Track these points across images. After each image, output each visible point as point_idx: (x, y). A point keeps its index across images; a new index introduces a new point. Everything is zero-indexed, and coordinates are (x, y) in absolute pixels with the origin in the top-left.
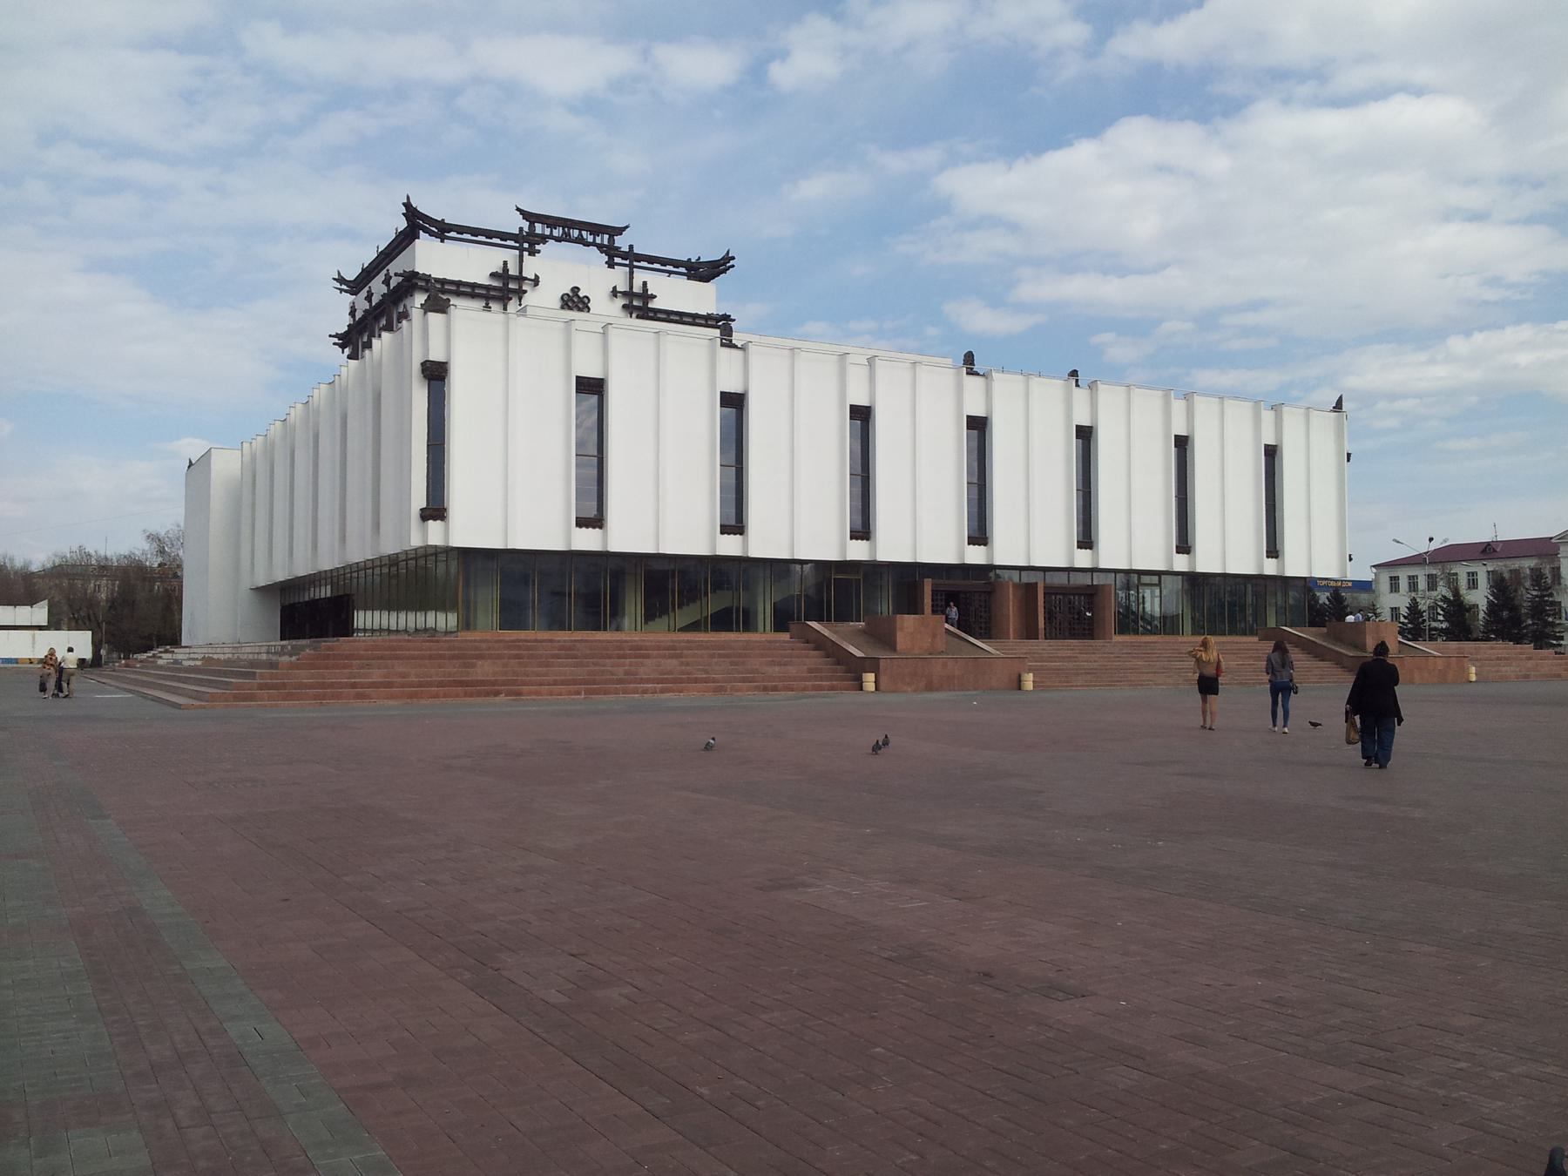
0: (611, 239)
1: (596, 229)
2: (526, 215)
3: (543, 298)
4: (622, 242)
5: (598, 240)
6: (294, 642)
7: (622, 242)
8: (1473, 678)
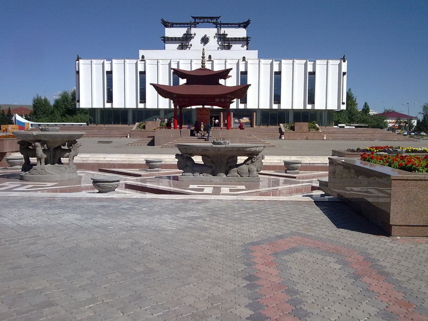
0: (217, 20)
1: (212, 18)
2: (193, 17)
3: (196, 42)
4: (219, 21)
5: (213, 21)
6: (107, 126)
7: (219, 21)
8: (325, 138)
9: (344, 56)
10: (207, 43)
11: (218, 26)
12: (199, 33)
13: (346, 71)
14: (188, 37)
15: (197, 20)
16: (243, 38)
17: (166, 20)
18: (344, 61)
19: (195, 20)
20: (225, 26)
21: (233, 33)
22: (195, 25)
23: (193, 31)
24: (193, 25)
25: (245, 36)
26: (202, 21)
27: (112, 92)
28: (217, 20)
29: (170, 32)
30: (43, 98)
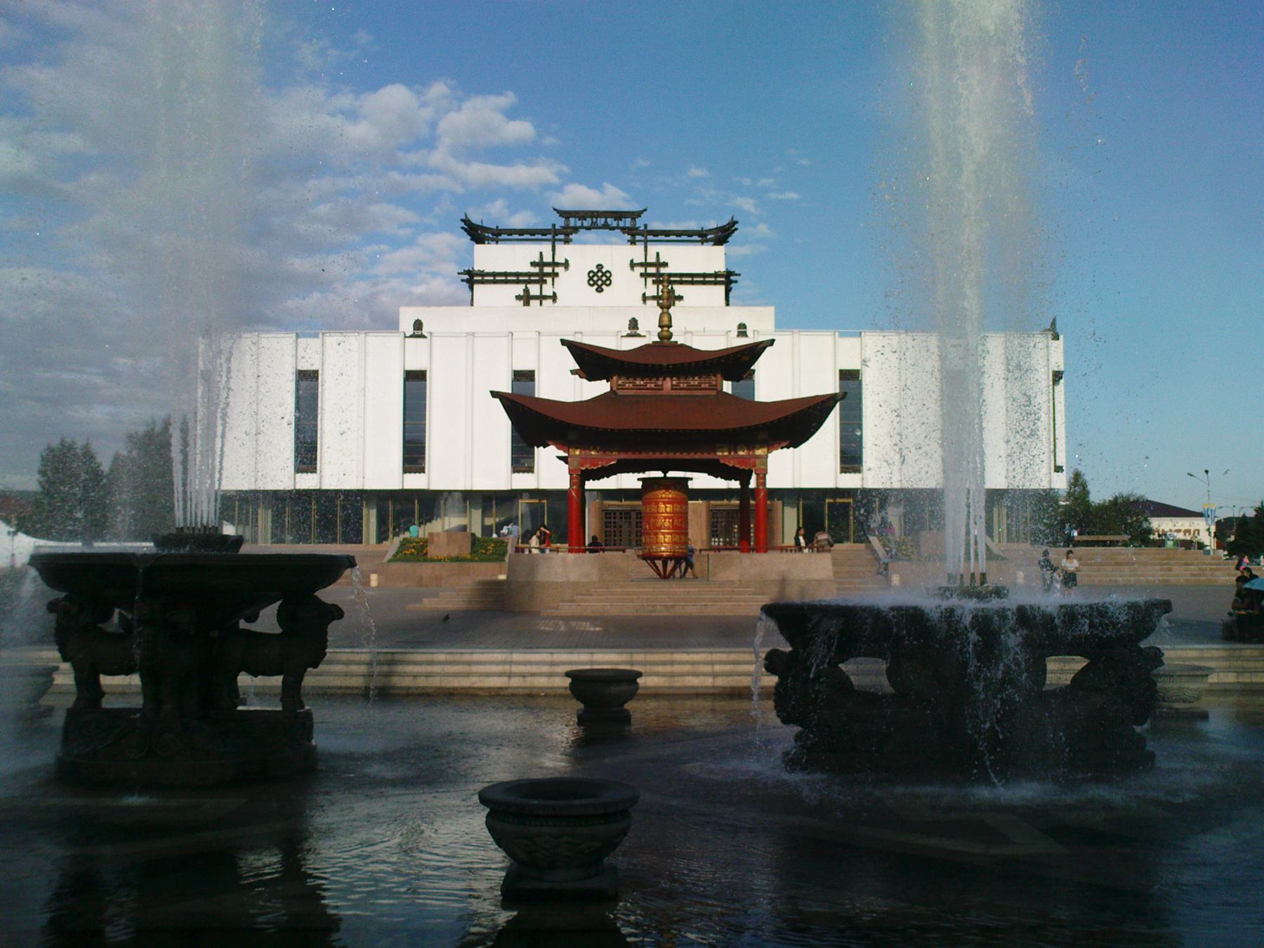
1: (619, 215)
4: (640, 223)
5: (621, 224)
7: (640, 223)
9: (1053, 324)
11: (638, 238)
12: (581, 255)
13: (1062, 369)
14: (543, 272)
16: (716, 275)
17: (476, 219)
18: (1056, 337)
20: (526, 236)
21: (681, 258)
22: (563, 234)
23: (563, 252)
24: (562, 237)
25: (721, 267)
26: (587, 223)
27: (861, 437)
29: (489, 257)
30: (80, 443)
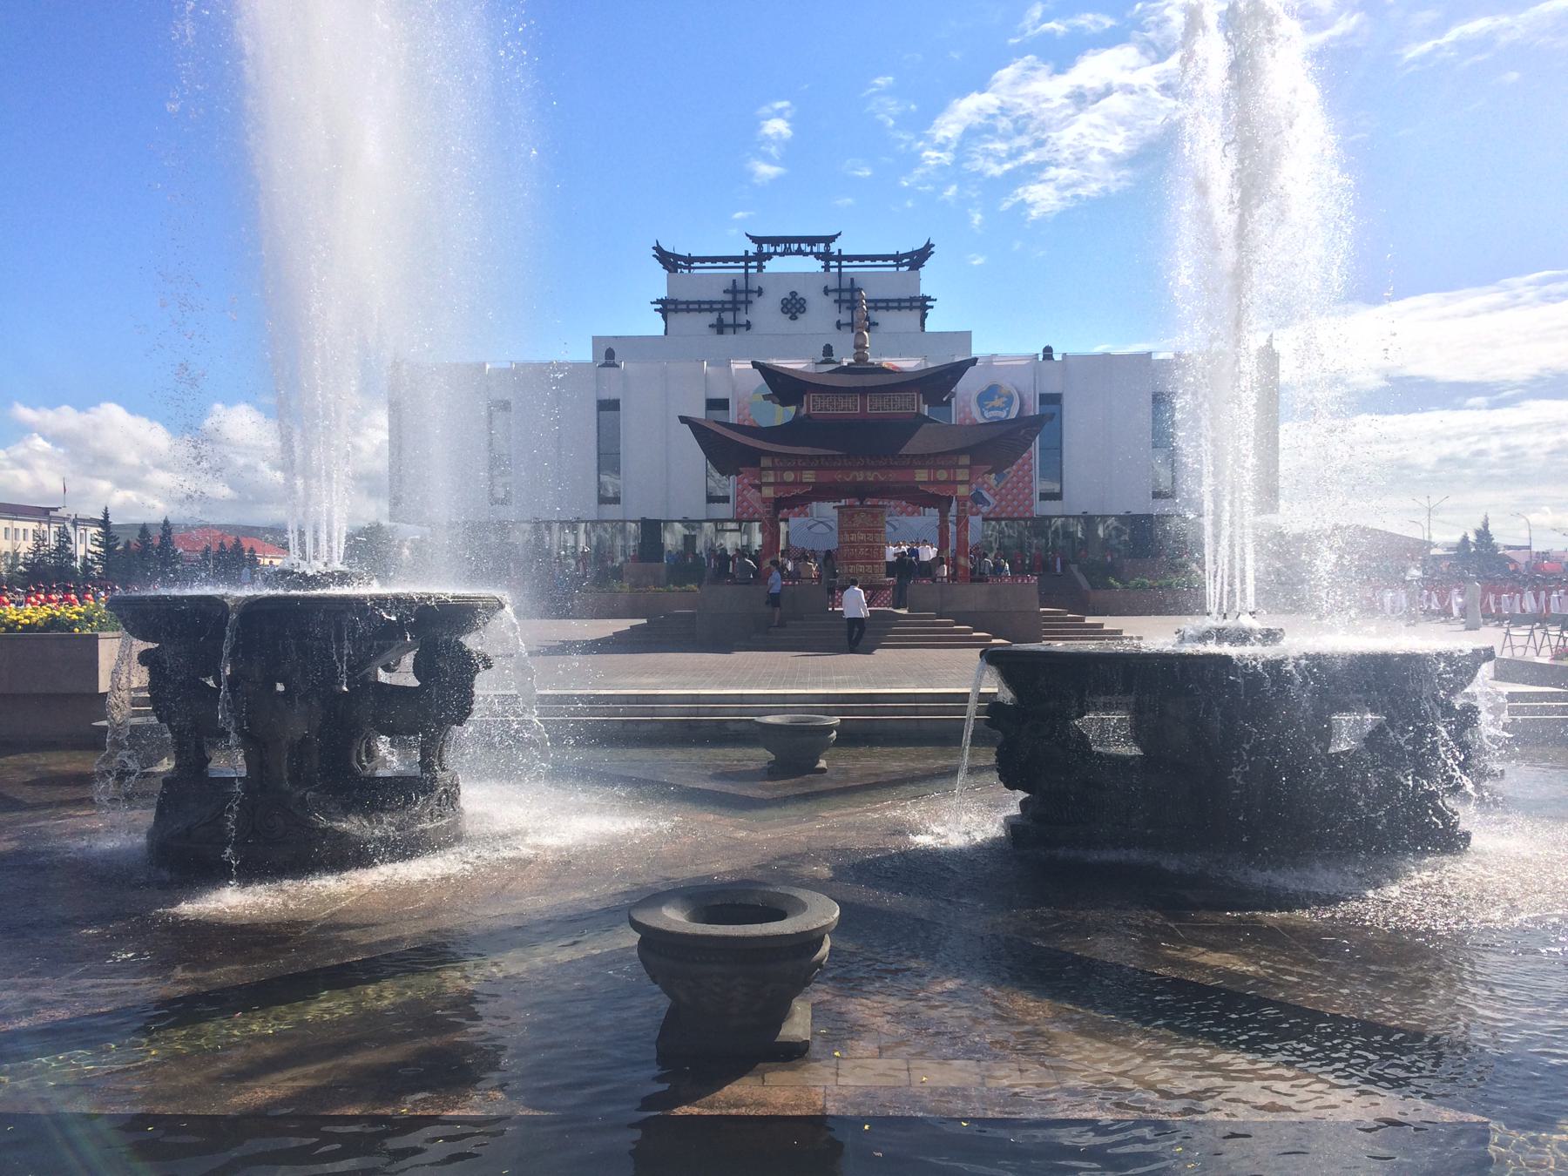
1: (812, 241)
2: (755, 239)
4: (834, 248)
5: (815, 249)
10: (1378, 301)
11: (832, 263)
15: (765, 246)
17: (667, 248)
19: (760, 247)
28: (827, 246)
